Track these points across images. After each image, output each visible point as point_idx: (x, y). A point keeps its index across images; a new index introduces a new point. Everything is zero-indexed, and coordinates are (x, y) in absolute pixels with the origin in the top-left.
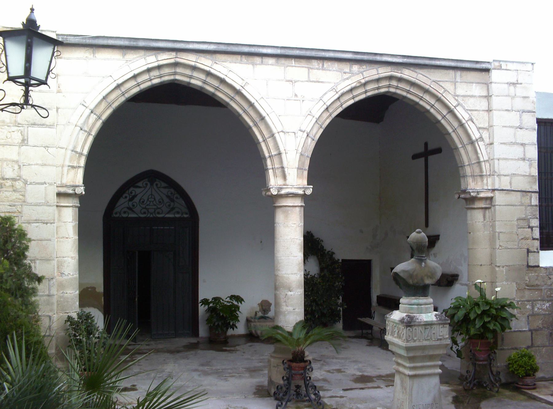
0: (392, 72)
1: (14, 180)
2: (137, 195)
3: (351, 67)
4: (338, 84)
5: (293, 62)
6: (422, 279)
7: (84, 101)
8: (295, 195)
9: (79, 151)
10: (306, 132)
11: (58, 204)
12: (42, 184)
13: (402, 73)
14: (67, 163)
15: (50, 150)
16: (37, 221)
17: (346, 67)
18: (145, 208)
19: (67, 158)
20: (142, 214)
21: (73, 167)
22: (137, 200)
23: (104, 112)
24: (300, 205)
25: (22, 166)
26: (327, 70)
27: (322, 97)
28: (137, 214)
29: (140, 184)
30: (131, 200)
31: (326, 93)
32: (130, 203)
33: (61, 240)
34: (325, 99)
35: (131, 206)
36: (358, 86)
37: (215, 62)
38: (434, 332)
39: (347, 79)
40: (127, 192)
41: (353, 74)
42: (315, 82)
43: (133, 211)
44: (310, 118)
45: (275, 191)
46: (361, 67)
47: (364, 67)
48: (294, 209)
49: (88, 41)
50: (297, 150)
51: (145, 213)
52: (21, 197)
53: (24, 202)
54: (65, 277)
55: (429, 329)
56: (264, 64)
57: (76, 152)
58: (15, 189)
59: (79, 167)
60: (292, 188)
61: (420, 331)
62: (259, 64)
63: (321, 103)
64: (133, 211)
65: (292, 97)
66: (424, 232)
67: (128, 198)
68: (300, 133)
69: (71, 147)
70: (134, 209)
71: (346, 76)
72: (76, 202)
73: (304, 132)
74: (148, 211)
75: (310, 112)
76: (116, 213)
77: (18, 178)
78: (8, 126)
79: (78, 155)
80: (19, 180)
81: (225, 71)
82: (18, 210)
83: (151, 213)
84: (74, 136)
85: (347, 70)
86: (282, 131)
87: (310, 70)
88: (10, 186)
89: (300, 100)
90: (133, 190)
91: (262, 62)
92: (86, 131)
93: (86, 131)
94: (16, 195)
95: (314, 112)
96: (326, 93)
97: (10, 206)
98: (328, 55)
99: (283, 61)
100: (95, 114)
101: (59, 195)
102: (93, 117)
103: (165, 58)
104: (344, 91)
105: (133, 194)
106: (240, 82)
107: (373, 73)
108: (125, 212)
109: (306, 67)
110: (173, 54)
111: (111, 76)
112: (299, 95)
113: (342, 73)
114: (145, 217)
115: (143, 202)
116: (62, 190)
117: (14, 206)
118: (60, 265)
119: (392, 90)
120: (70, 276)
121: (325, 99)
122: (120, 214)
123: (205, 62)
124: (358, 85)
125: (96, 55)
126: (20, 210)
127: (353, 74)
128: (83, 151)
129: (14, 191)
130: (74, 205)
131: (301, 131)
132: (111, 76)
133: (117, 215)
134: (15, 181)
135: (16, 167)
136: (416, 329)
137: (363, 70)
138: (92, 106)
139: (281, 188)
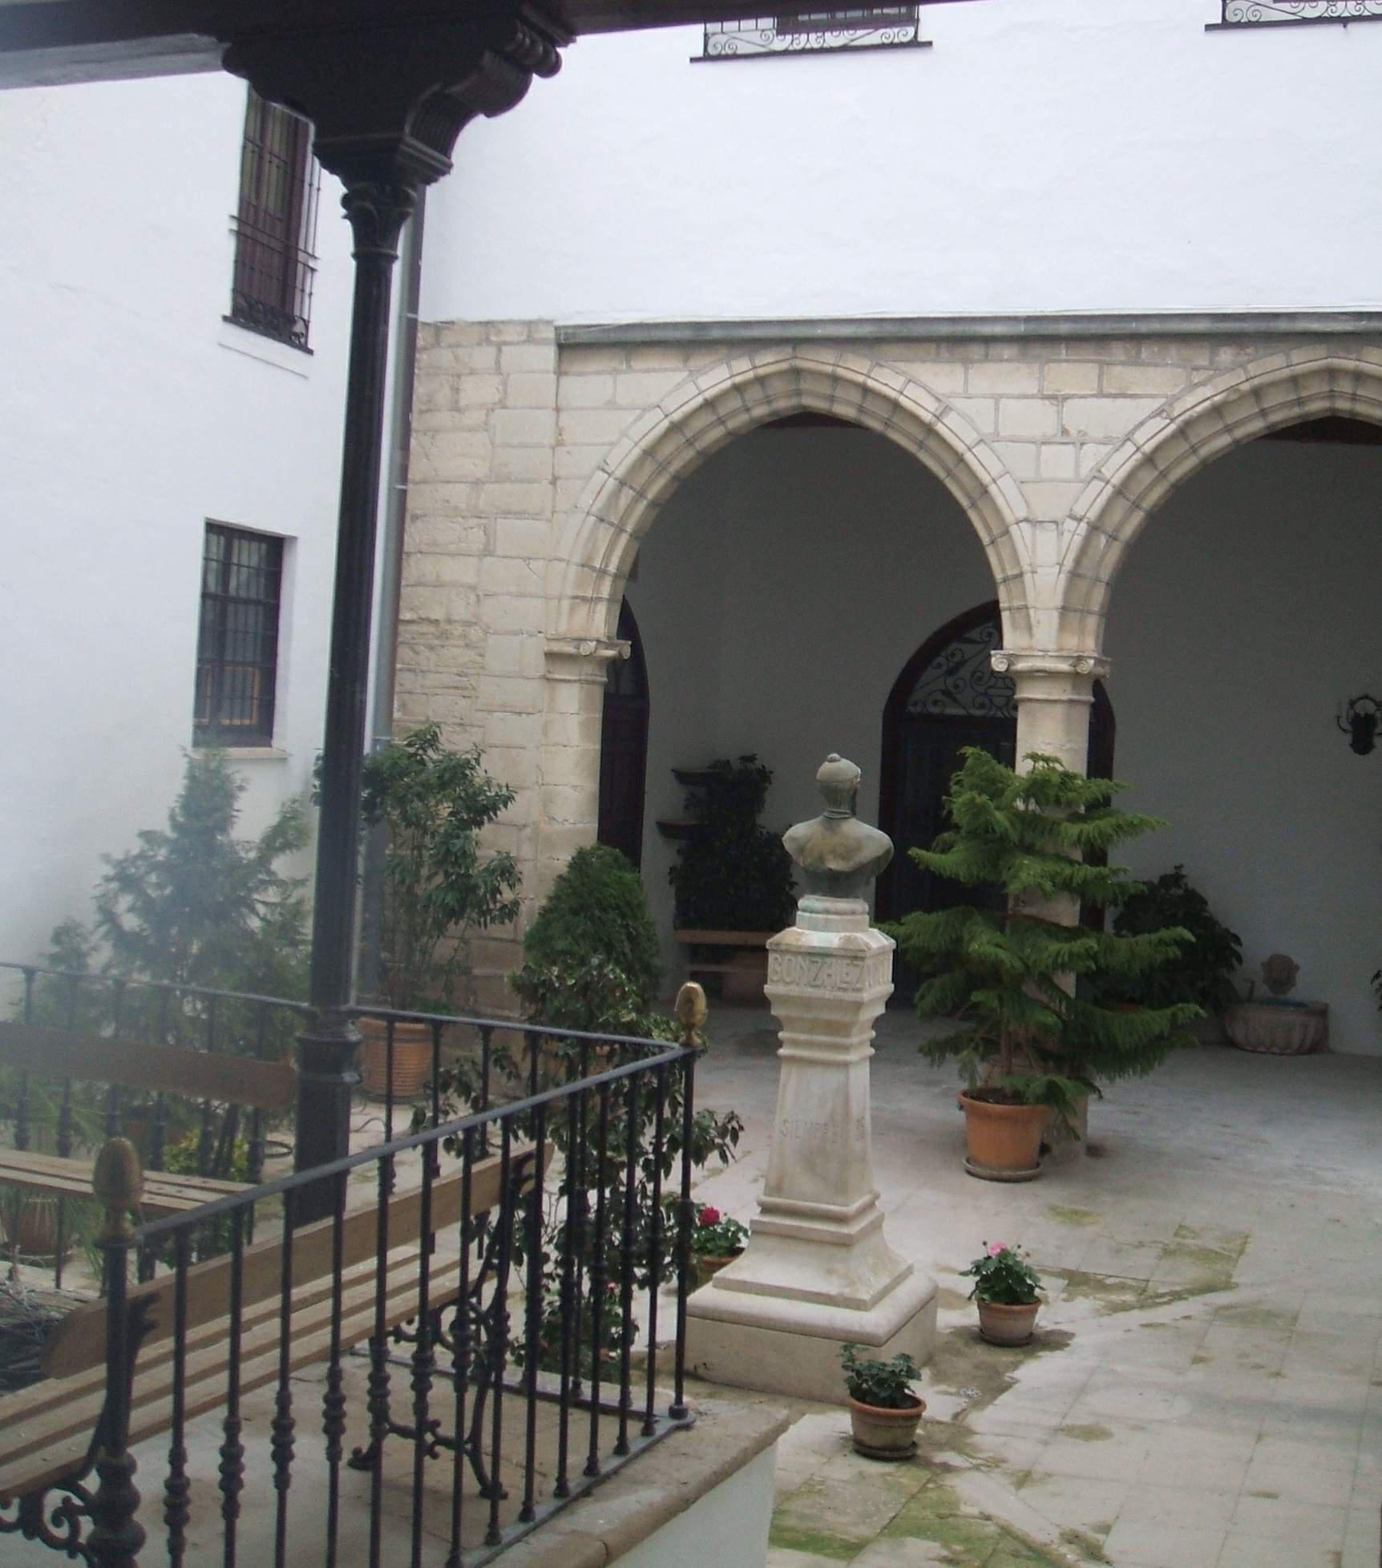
0: (1330, 360)
1: (468, 624)
2: (966, 661)
3: (1214, 353)
4: (1177, 398)
5: (1064, 351)
6: (821, 859)
7: (605, 461)
8: (1052, 675)
9: (598, 566)
10: (1086, 520)
11: (549, 676)
12: (515, 633)
13: (1359, 360)
14: (569, 592)
15: (533, 564)
16: (504, 708)
17: (1201, 356)
18: (985, 694)
19: (566, 579)
20: (978, 708)
21: (584, 599)
22: (965, 672)
23: (650, 482)
24: (1065, 697)
25: (482, 597)
26: (1148, 365)
27: (1133, 432)
28: (965, 709)
29: (974, 634)
30: (951, 672)
31: (1142, 424)
32: (950, 681)
33: (554, 748)
34: (1140, 437)
35: (951, 689)
36: (1234, 401)
37: (877, 364)
38: (829, 972)
39: (1203, 384)
40: (943, 654)
41: (1220, 370)
42: (1115, 396)
43: (955, 700)
44: (1097, 485)
45: (1002, 662)
46: (1242, 352)
47: (1250, 350)
48: (1048, 708)
49: (613, 337)
50: (1061, 565)
51: (982, 706)
52: (479, 659)
53: (483, 668)
54: (557, 827)
55: (819, 964)
56: (990, 361)
57: (593, 568)
58: (468, 642)
59: (599, 599)
60: (1044, 656)
61: (798, 967)
62: (980, 361)
63: (1129, 448)
64: (955, 700)
65: (1055, 435)
66: (847, 758)
67: (944, 668)
68: (1070, 524)
69: (577, 558)
70: (959, 697)
71: (1197, 377)
72: (591, 672)
73: (1080, 520)
74: (991, 700)
75: (1099, 471)
76: (915, 704)
77: (474, 621)
78: (463, 517)
79: (595, 575)
80: (475, 623)
81: (897, 382)
82: (471, 685)
83: (1000, 708)
84: (585, 534)
85: (1203, 361)
86: (1026, 520)
87: (1105, 367)
88: (460, 636)
89: (1073, 443)
90: (956, 649)
91: (987, 356)
92: (611, 524)
93: (611, 524)
94: (470, 655)
95: (1107, 472)
96: (1142, 424)
97: (460, 675)
98: (1144, 328)
99: (1037, 350)
100: (631, 488)
101: (551, 656)
102: (627, 495)
103: (769, 362)
104: (1191, 416)
105: (957, 659)
106: (932, 405)
107: (1272, 365)
108: (935, 703)
109: (1092, 361)
110: (788, 351)
111: (659, 407)
112: (1073, 432)
113: (1189, 370)
114: (984, 717)
115: (980, 679)
116: (556, 647)
117: (466, 675)
118: (547, 801)
119: (1343, 405)
120: (567, 826)
121: (1140, 437)
122: (925, 704)
123: (856, 367)
124: (1234, 397)
125: (632, 363)
126: (474, 685)
127: (1219, 371)
128: (606, 566)
129: (467, 645)
130: (583, 677)
131: (1072, 517)
132: (659, 407)
133: (919, 709)
134: (469, 626)
135: (473, 598)
136: (790, 960)
137: (1247, 358)
138: (620, 472)
139: (1017, 656)
